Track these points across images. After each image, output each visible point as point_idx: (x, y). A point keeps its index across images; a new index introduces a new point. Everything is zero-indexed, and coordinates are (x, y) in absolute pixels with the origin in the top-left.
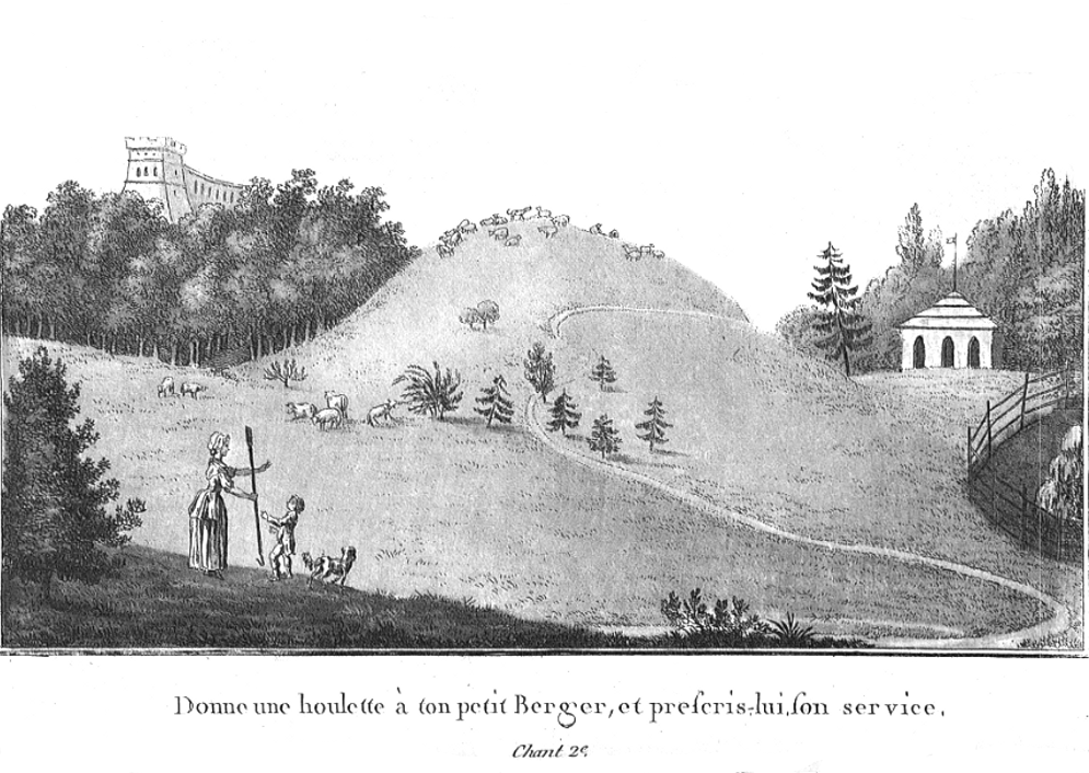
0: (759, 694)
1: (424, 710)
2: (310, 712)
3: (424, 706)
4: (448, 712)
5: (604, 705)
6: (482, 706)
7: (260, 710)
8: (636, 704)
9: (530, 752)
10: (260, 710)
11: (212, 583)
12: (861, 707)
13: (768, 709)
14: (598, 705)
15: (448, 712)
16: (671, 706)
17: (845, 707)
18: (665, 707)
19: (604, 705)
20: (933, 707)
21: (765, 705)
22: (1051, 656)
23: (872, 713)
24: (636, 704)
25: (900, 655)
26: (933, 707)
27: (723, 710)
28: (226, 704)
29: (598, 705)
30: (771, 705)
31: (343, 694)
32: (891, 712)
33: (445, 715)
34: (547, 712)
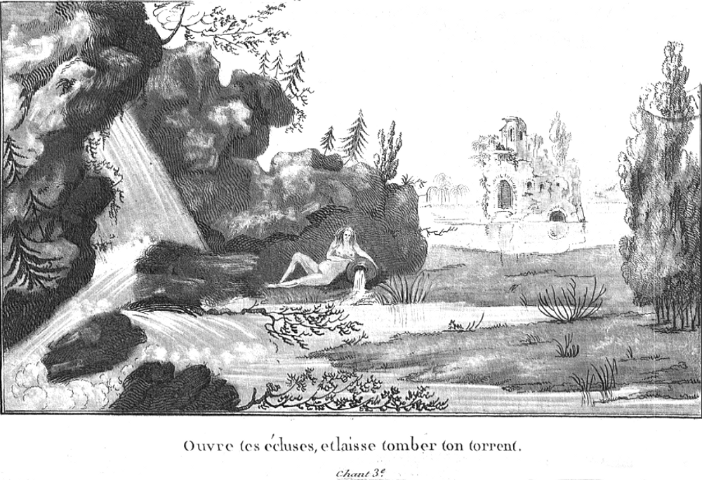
0: (338, 438)
1: (445, 448)
2: (510, 450)
3: (445, 445)
4: (462, 449)
5: (435, 444)
6: (329, 446)
7: (459, 446)
8: (331, 445)
9: (347, 474)
10: (459, 446)
11: (415, 370)
12: (425, 445)
13: (288, 448)
14: (431, 444)
15: (462, 449)
16: (221, 446)
17: (259, 449)
18: (482, 446)
19: (435, 444)
20: (232, 446)
21: (285, 445)
22: (631, 417)
23: (432, 449)
24: (331, 445)
25: (275, 415)
26: (232, 446)
27: (495, 448)
28: (510, 450)
29: (431, 444)
30: (350, 445)
31: (412, 437)
32: (211, 449)
33: (459, 451)
34: (432, 449)
